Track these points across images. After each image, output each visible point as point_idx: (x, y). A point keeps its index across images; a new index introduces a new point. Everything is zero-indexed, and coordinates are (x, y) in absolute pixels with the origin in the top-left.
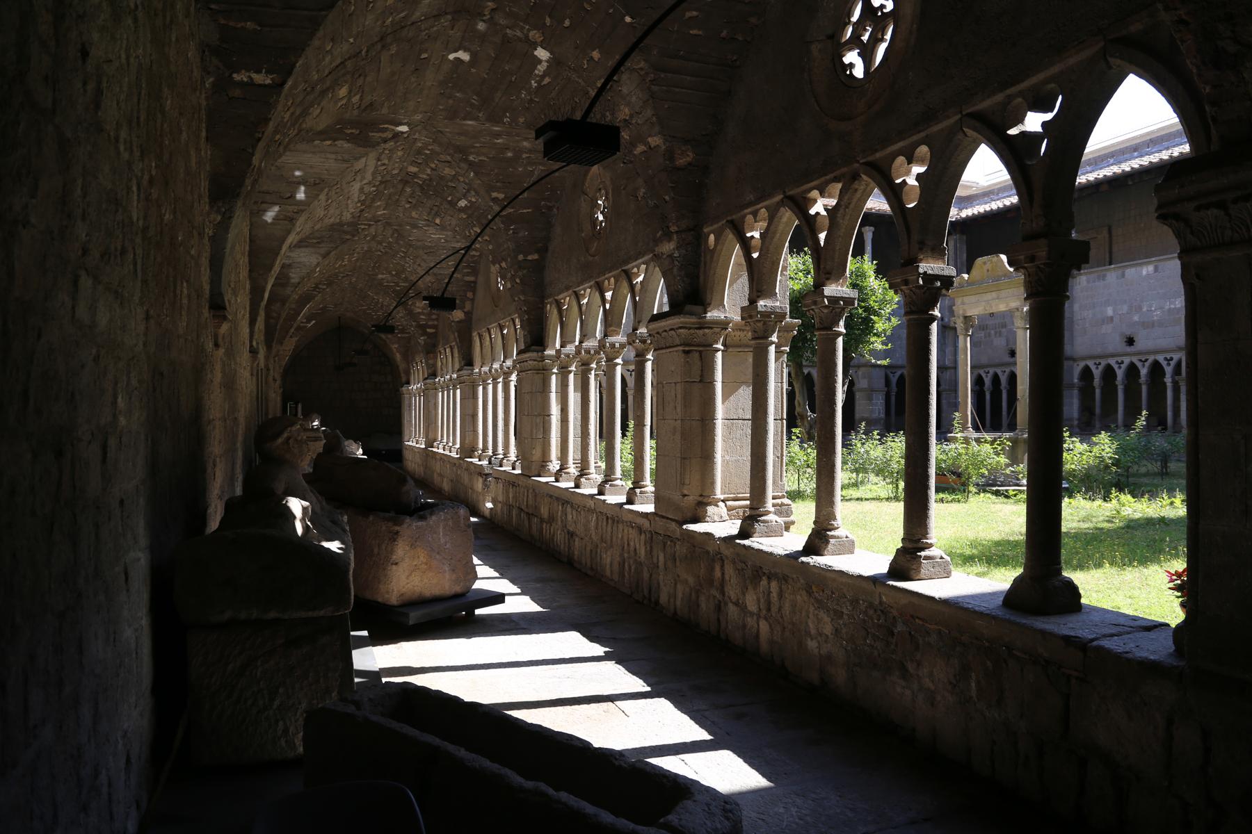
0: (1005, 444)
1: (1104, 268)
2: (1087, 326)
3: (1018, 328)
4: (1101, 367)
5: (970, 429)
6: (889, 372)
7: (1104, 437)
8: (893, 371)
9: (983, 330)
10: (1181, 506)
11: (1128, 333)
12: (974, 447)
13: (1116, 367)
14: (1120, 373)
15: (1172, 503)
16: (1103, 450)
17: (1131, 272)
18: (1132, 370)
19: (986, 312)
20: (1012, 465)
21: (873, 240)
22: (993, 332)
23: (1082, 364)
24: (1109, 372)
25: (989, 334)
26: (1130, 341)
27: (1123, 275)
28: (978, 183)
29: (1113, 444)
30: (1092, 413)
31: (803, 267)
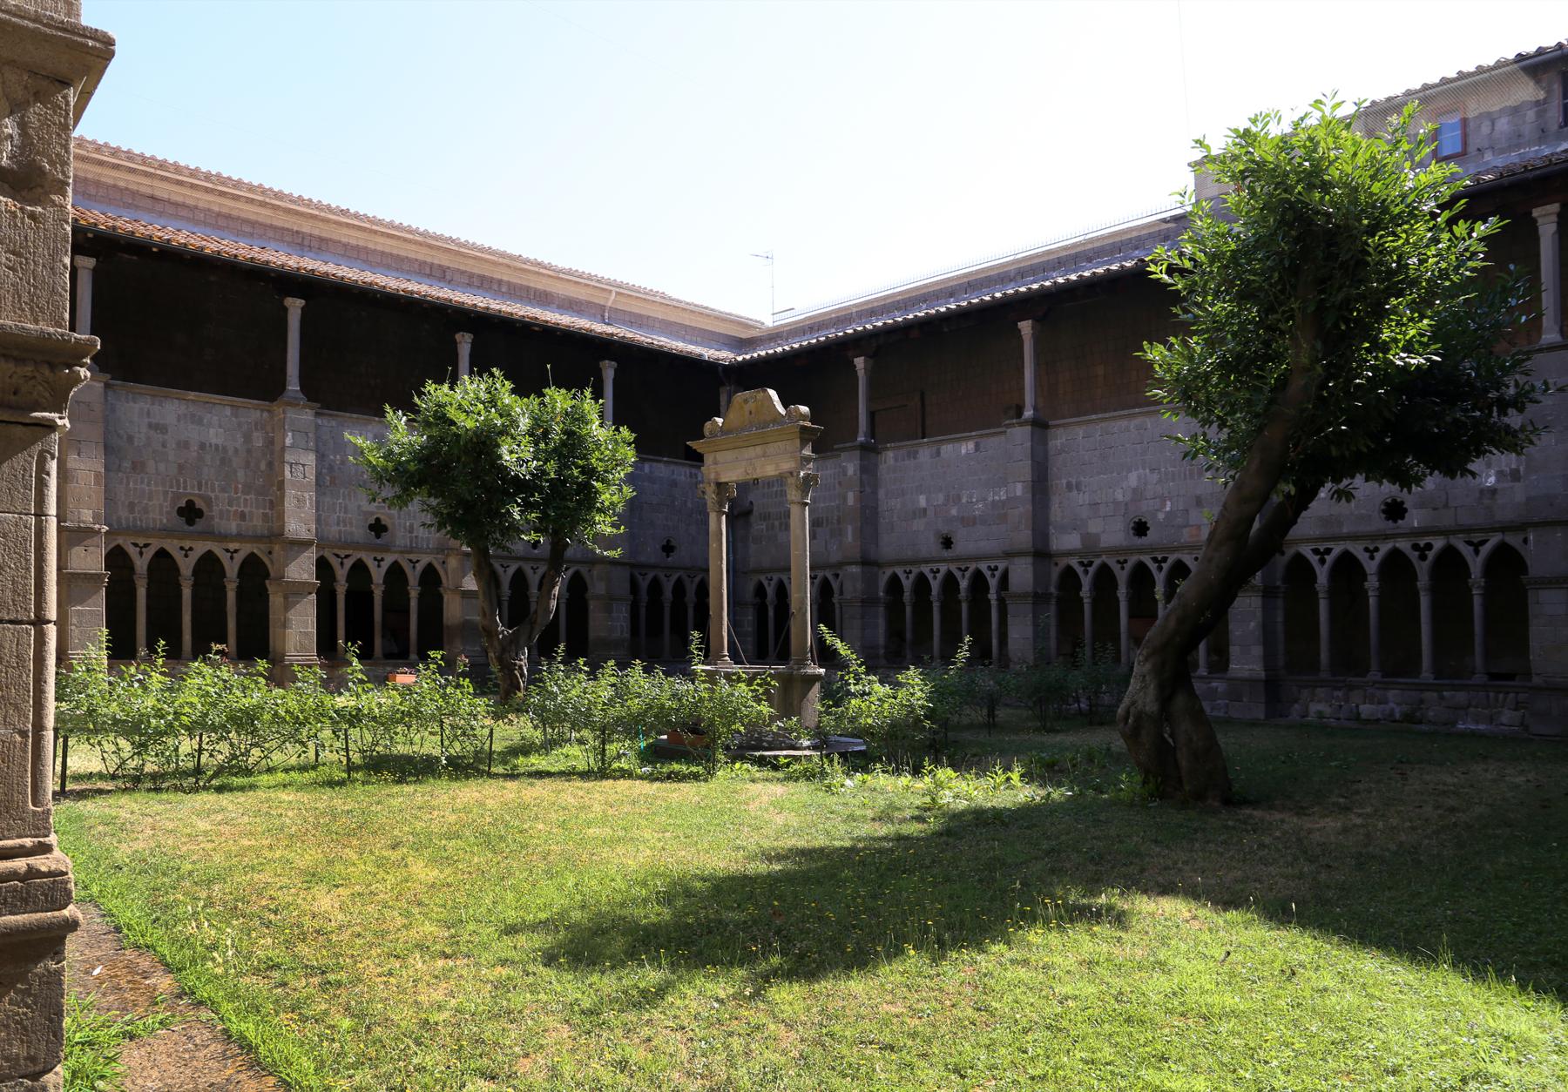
0: (769, 684)
1: (916, 442)
2: (895, 519)
3: (793, 502)
4: (912, 577)
5: (727, 658)
6: (636, 574)
7: (912, 676)
8: (643, 572)
9: (765, 520)
10: (1020, 784)
11: (945, 530)
12: (724, 688)
13: (930, 576)
14: (935, 586)
15: (1008, 779)
16: (913, 694)
17: (947, 449)
18: (950, 582)
19: (748, 477)
20: (780, 719)
21: (615, 380)
22: (777, 523)
23: (889, 572)
24: (922, 583)
25: (773, 525)
26: (947, 543)
27: (938, 453)
28: (763, 324)
29: (926, 685)
30: (903, 639)
31: (488, 396)
